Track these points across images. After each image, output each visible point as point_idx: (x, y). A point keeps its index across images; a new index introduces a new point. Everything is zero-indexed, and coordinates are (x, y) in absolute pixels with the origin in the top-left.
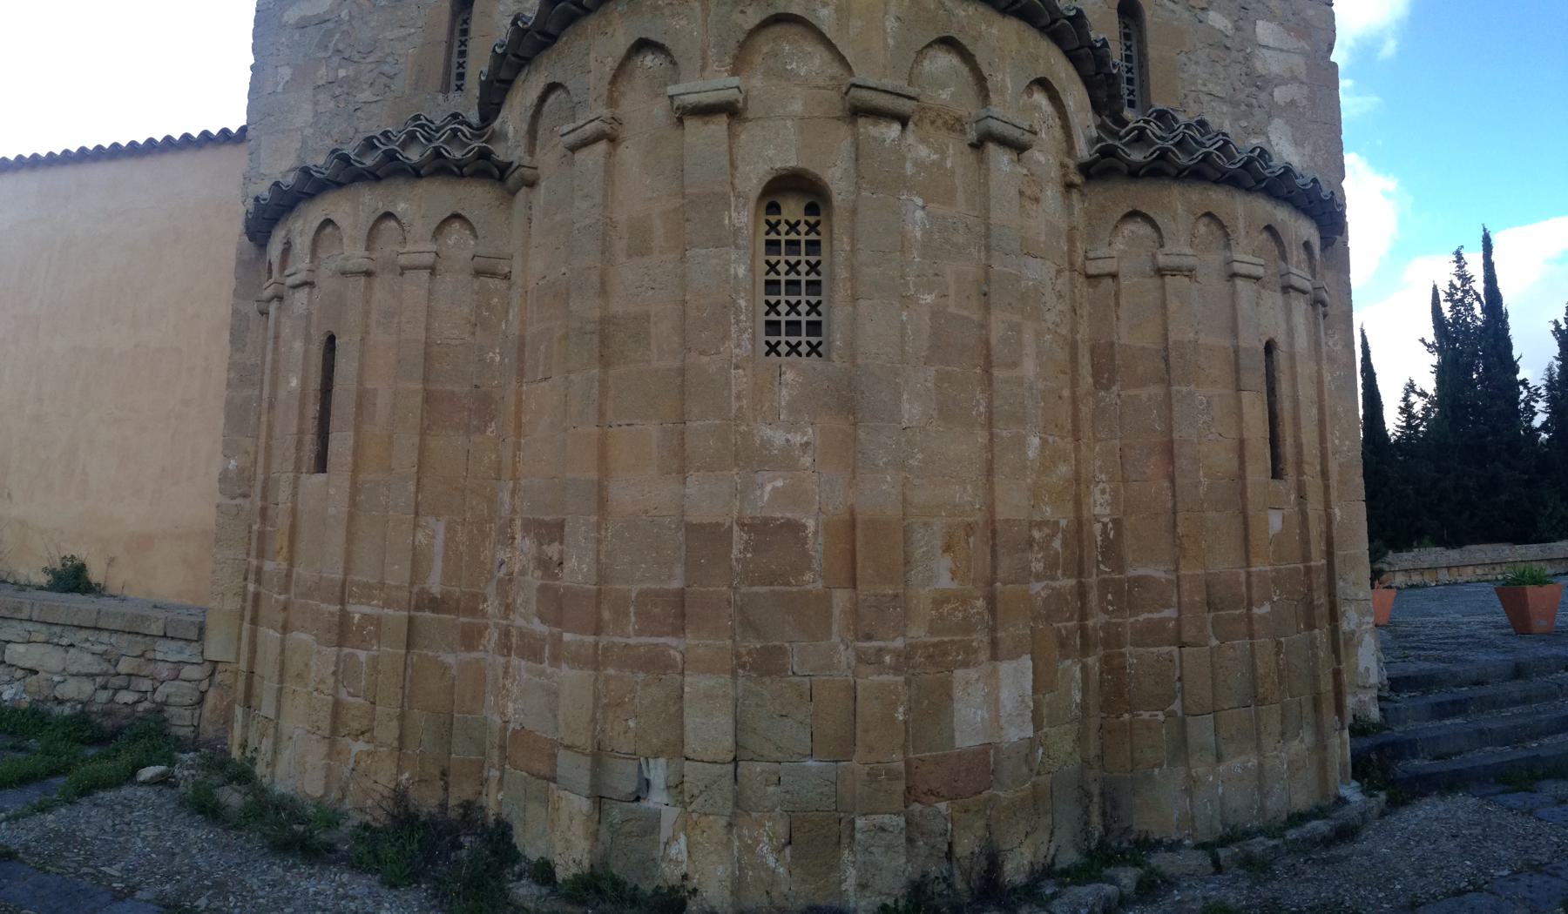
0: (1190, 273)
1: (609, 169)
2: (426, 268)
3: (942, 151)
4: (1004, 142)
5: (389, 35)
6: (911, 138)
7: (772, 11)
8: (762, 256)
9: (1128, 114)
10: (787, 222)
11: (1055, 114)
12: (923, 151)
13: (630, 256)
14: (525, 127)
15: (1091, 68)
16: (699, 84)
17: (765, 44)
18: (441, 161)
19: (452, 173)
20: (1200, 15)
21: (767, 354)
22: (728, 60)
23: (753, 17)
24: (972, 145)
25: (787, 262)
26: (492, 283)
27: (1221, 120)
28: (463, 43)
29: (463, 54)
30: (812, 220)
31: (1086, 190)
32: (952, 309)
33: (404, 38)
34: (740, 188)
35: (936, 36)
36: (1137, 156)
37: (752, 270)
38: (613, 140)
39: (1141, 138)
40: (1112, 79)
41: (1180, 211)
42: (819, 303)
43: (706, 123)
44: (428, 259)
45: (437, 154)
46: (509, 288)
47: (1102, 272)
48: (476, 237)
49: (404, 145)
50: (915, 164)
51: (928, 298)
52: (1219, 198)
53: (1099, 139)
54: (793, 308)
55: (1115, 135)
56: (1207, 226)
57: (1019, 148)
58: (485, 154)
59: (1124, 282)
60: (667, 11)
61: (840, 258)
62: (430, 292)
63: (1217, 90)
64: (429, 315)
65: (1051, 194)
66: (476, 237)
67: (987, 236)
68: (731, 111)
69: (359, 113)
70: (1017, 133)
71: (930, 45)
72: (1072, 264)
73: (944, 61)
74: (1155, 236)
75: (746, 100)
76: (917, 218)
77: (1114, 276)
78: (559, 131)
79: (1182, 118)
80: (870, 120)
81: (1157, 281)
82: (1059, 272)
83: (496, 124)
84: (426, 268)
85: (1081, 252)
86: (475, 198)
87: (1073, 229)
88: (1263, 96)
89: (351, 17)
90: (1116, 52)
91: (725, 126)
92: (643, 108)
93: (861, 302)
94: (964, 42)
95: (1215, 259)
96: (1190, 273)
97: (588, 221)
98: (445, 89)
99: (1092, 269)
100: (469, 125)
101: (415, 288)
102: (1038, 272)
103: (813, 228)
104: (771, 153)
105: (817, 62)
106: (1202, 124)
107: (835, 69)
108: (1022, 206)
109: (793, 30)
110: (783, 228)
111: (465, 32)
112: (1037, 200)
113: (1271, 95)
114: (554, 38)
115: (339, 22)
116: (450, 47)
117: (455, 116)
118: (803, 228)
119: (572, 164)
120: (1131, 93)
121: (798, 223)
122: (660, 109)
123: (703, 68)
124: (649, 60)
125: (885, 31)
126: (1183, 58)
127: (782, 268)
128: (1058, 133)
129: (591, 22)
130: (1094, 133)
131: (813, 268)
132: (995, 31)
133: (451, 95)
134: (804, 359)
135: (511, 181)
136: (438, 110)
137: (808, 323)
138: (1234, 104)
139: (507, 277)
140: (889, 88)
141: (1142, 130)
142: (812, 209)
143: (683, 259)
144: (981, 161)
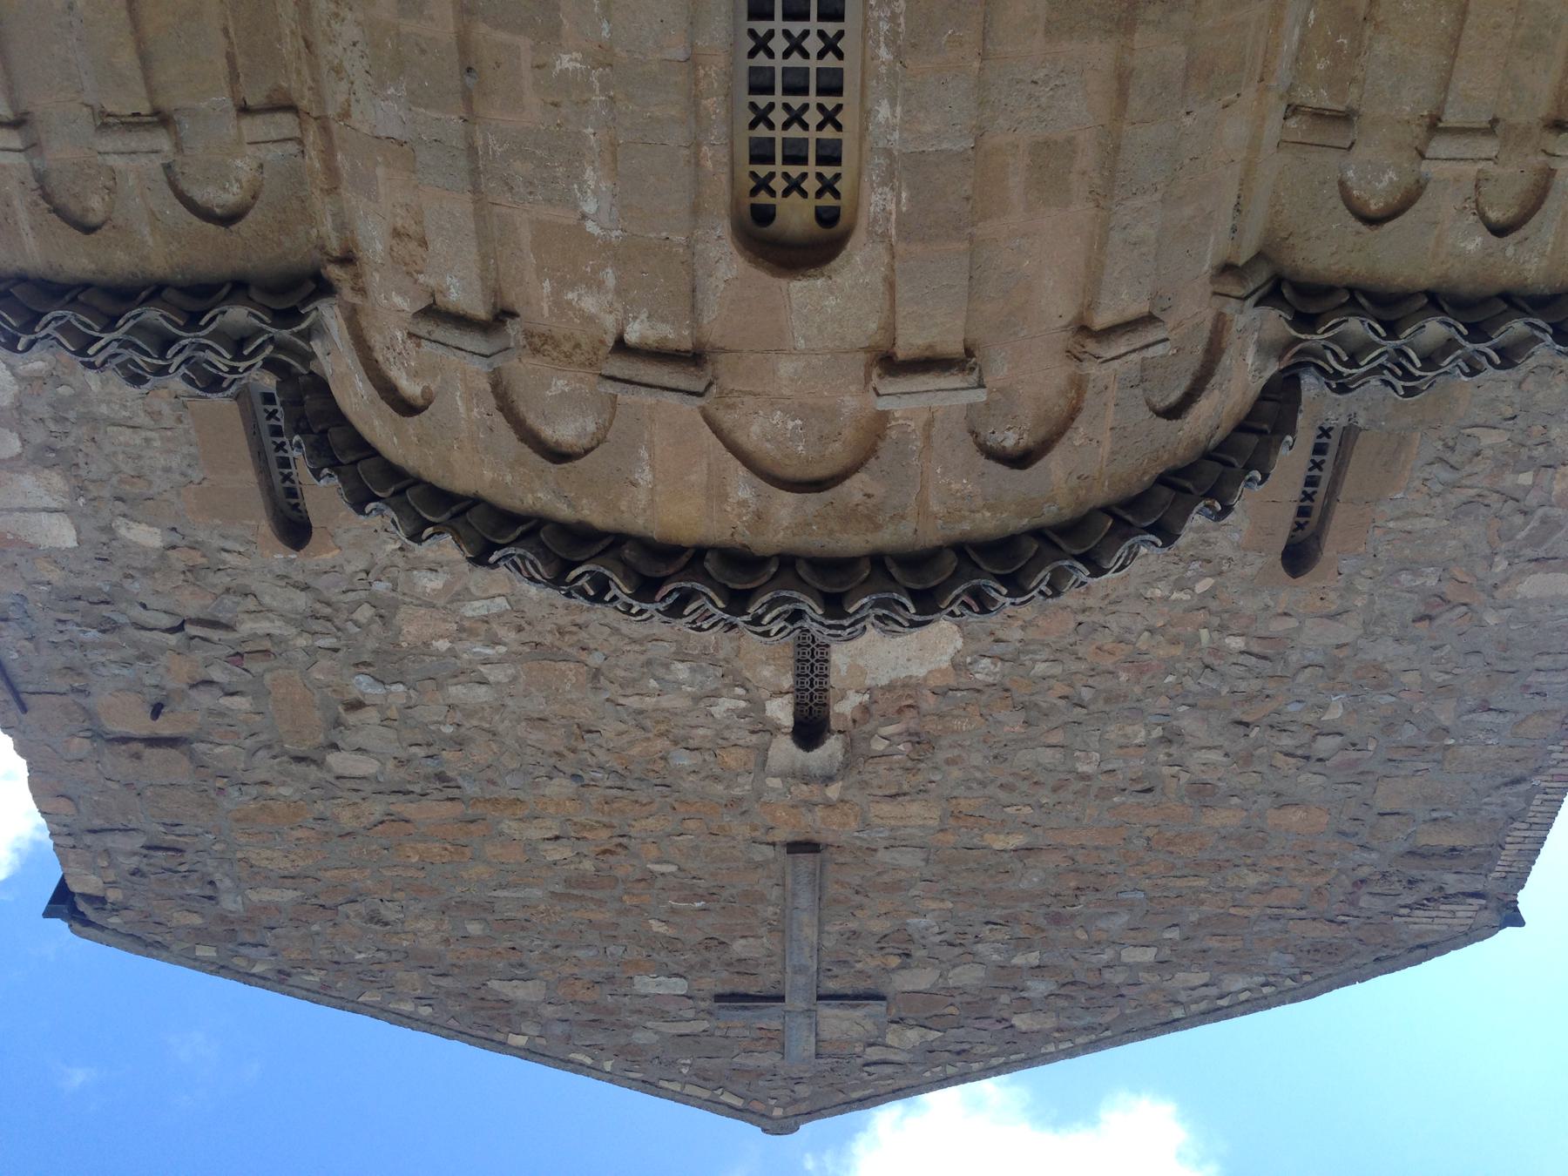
0: (105, 122)
1: (1092, 284)
2: (1447, 130)
3: (559, 305)
4: (461, 321)
5: (1431, 523)
6: (609, 322)
7: (827, 495)
8: (848, 138)
9: (269, 382)
10: (804, 194)
11: (384, 367)
12: (589, 304)
13: (1070, 141)
14: (1226, 360)
15: (336, 436)
16: (937, 401)
17: (837, 454)
18: (1386, 316)
19: (1367, 294)
20: (175, 538)
22: (893, 434)
23: (854, 488)
24: (513, 315)
25: (805, 126)
26: (1324, 99)
27: (103, 389)
28: (1308, 496)
29: (1311, 482)
30: (763, 198)
31: (317, 255)
32: (524, 42)
33: (1407, 515)
34: (881, 248)
35: (577, 463)
36: (237, 315)
37: (866, 114)
38: (1083, 329)
39: (238, 344)
40: (301, 425)
41: (146, 231)
42: (752, 54)
43: (930, 346)
44: (1441, 147)
45: (1392, 329)
46: (1291, 88)
47: (268, 117)
48: (1342, 184)
49: (1449, 346)
50: (601, 285)
51: (567, 62)
52: (77, 259)
53: (307, 335)
54: (796, 45)
55: (280, 346)
56: (86, 210)
57: (434, 312)
58: (1306, 321)
59: (224, 100)
60: (979, 502)
61: (717, 133)
62: (1445, 85)
63: (125, 435)
64: (1456, 40)
65: (374, 244)
66: (1342, 184)
67: (475, 172)
68: (890, 364)
69: (1509, 412)
70: (440, 333)
71: (587, 451)
72: (325, 129)
73: (564, 432)
74: (184, 185)
75: (868, 378)
76: (594, 201)
77: (244, 110)
78: (1169, 354)
79: (176, 384)
80: (672, 346)
81: (163, 102)
82: (345, 115)
83: (1273, 368)
84: (1447, 130)
85: (312, 153)
86: (1332, 250)
87: (332, 190)
88: (38, 436)
89: (1490, 561)
90: (302, 471)
91: (900, 342)
92: (1029, 375)
93: (680, 54)
94: (537, 458)
95: (61, 152)
96: (105, 122)
97: (1138, 202)
98: (1350, 433)
99: (285, 123)
101: (1474, 94)
102: (381, 113)
103: (763, 185)
104: (831, 301)
105: (755, 429)
106: (136, 379)
107: (727, 419)
109: (792, 471)
110: (811, 185)
111: (1303, 512)
112: (397, 234)
113: (24, 441)
114: (1162, 480)
115: (1512, 557)
116: (1332, 494)
117: (1343, 389)
118: (779, 184)
119: (1155, 297)
120: (272, 415)
121: (786, 193)
122: (999, 370)
123: (929, 424)
124: (1010, 440)
125: (653, 468)
126: (196, 475)
127: (813, 117)
128: (376, 340)
129: (1101, 494)
130: (317, 346)
131: (761, 117)
132: (488, 474)
133: (1344, 422)
135: (1262, 276)
136: (1372, 401)
137: (770, 17)
138: (92, 420)
139: (1293, 110)
140: (643, 389)
141: (238, 356)
142: (764, 215)
143: (980, 133)
144: (497, 292)
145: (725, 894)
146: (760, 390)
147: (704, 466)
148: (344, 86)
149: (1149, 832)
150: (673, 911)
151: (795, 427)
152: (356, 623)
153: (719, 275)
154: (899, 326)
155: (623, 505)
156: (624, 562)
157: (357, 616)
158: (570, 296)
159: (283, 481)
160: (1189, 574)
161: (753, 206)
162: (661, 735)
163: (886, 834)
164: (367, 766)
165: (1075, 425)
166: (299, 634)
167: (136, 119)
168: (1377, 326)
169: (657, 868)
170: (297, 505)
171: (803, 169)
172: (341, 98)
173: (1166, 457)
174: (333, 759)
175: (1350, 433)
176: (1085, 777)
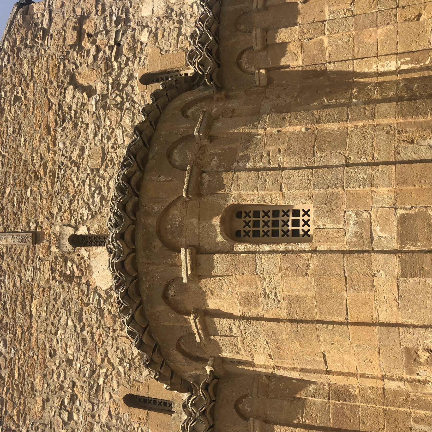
3: (214, 155)
10: (245, 227)
12: (213, 163)
14: (194, 363)
18: (208, 412)
21: (309, 210)
22: (173, 254)
23: (157, 243)
24: (211, 142)
25: (263, 227)
30: (243, 215)
41: (234, 40)
48: (247, 395)
50: (219, 167)
65: (230, 105)
74: (247, 52)
82: (267, 98)
98: (171, 412)
100: (190, 398)
103: (247, 215)
105: (176, 212)
108: (236, 116)
110: (247, 229)
112: (234, 110)
117: (185, 406)
118: (247, 219)
121: (245, 222)
125: (164, 181)
132: (163, 133)
133: (174, 409)
134: (311, 218)
142: (239, 215)
145: (19, 213)
146: (188, 213)
147: (165, 197)
148: (274, 98)
149: (35, 357)
150: (14, 195)
151: (176, 224)
152: (116, 97)
153: (222, 201)
154: (206, 255)
155: (153, 172)
156: (135, 172)
157: (118, 97)
158: (216, 158)
159: (161, 78)
160: (125, 364)
161: (241, 212)
162: (76, 191)
163: (38, 267)
164: (68, 99)
165: (175, 313)
166: (113, 79)
167: (265, 40)
168: (204, 409)
169: (29, 190)
170: (154, 82)
171: (252, 217)
172: (271, 97)
173: (164, 345)
174: (71, 87)
175: (171, 412)
176: (56, 334)
